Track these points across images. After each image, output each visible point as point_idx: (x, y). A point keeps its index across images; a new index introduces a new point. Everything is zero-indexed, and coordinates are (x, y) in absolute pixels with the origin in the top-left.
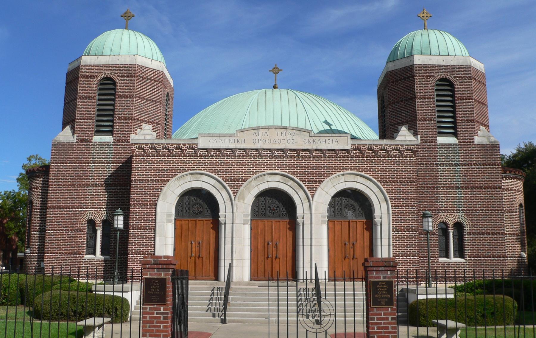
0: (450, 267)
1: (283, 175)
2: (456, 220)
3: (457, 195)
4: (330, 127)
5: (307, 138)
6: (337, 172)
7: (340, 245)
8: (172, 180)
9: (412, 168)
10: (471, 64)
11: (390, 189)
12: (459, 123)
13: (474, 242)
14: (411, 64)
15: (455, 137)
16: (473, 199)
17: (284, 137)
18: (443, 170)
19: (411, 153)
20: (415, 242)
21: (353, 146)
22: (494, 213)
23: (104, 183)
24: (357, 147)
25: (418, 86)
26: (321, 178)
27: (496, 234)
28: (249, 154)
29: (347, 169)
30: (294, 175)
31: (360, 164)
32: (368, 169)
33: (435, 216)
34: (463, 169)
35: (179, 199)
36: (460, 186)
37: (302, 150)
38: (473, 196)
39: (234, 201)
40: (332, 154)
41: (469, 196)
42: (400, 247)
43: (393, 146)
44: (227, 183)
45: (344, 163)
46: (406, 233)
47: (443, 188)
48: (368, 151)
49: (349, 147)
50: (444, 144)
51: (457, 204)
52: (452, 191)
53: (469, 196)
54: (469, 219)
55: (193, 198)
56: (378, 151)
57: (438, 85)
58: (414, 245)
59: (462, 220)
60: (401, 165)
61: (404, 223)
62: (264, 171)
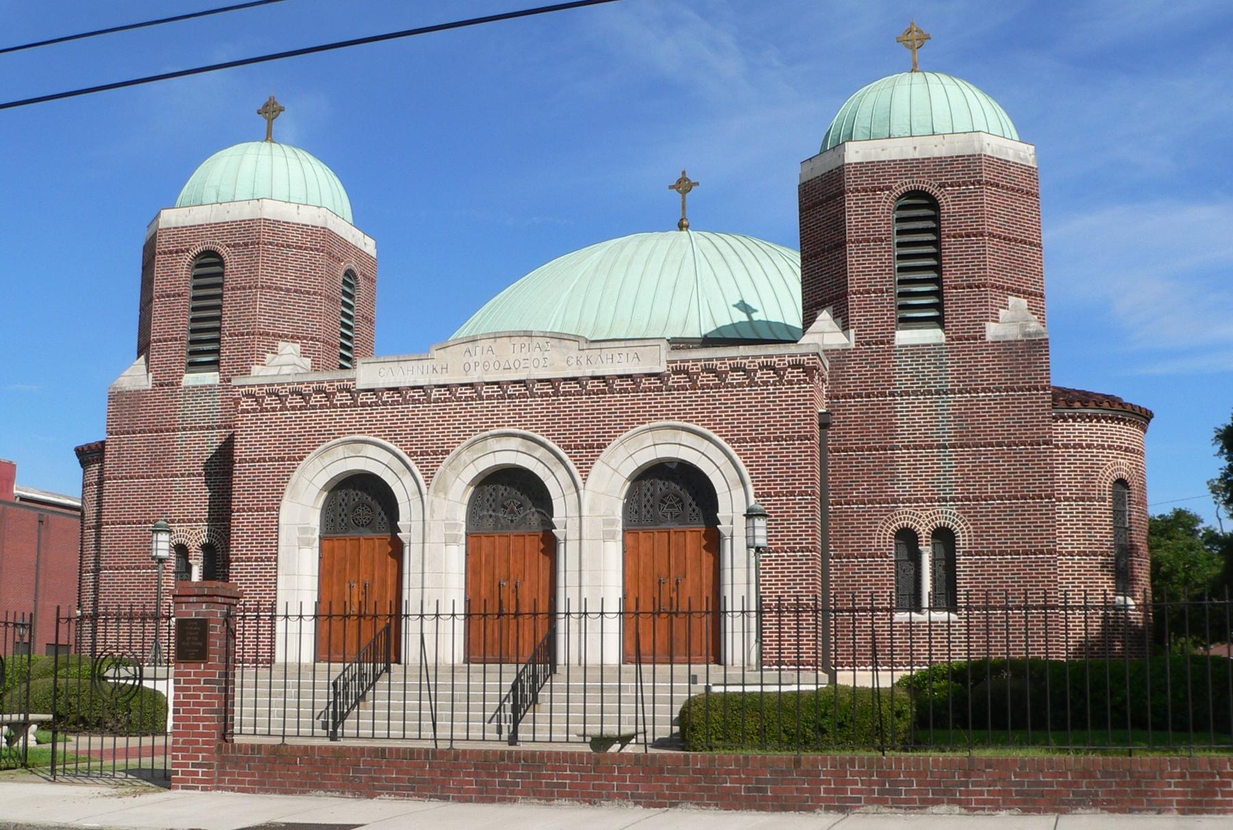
0: (921, 633)
1: (524, 437)
2: (937, 522)
3: (939, 464)
4: (749, 316)
5: (574, 353)
6: (638, 423)
7: (650, 583)
8: (309, 457)
9: (804, 408)
10: (982, 150)
11: (752, 458)
12: (950, 294)
13: (979, 572)
14: (840, 164)
15: (941, 328)
16: (978, 472)
17: (525, 354)
18: (908, 407)
19: (803, 372)
20: (806, 576)
21: (670, 365)
22: (1032, 504)
23: (204, 470)
24: (680, 366)
25: (852, 215)
26: (603, 440)
27: (1035, 554)
28: (458, 395)
29: (659, 416)
30: (547, 435)
31: (688, 403)
32: (706, 414)
33: (886, 515)
34: (957, 404)
35: (327, 498)
36: (947, 443)
37: (565, 379)
38: (980, 466)
39: (425, 497)
40: (627, 385)
41: (968, 466)
42: (773, 587)
43: (760, 360)
44: (415, 457)
45: (653, 405)
46: (788, 556)
47: (908, 449)
48: (705, 375)
49: (662, 368)
50: (911, 346)
51: (939, 486)
52: (928, 456)
53: (970, 465)
54: (969, 520)
55: (355, 493)
56: (727, 373)
57: (901, 208)
58: (804, 582)
59: (951, 523)
60: (780, 401)
61: (783, 532)
62: (487, 430)
